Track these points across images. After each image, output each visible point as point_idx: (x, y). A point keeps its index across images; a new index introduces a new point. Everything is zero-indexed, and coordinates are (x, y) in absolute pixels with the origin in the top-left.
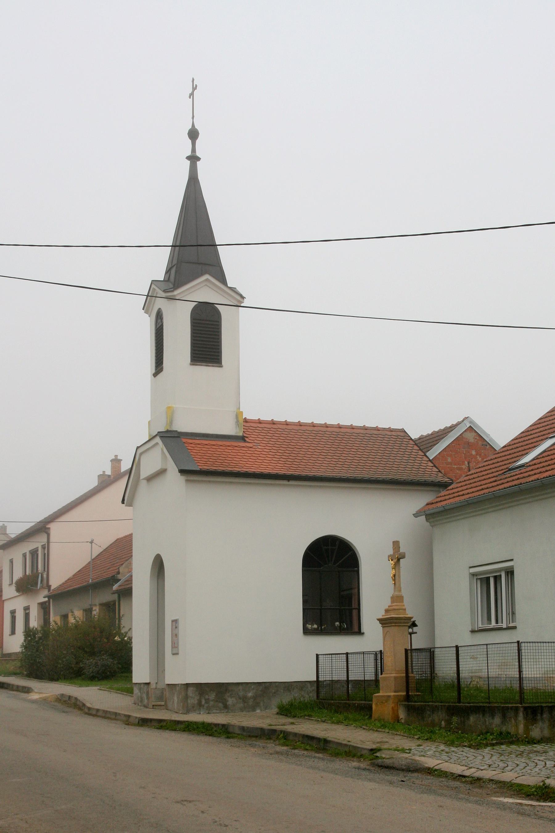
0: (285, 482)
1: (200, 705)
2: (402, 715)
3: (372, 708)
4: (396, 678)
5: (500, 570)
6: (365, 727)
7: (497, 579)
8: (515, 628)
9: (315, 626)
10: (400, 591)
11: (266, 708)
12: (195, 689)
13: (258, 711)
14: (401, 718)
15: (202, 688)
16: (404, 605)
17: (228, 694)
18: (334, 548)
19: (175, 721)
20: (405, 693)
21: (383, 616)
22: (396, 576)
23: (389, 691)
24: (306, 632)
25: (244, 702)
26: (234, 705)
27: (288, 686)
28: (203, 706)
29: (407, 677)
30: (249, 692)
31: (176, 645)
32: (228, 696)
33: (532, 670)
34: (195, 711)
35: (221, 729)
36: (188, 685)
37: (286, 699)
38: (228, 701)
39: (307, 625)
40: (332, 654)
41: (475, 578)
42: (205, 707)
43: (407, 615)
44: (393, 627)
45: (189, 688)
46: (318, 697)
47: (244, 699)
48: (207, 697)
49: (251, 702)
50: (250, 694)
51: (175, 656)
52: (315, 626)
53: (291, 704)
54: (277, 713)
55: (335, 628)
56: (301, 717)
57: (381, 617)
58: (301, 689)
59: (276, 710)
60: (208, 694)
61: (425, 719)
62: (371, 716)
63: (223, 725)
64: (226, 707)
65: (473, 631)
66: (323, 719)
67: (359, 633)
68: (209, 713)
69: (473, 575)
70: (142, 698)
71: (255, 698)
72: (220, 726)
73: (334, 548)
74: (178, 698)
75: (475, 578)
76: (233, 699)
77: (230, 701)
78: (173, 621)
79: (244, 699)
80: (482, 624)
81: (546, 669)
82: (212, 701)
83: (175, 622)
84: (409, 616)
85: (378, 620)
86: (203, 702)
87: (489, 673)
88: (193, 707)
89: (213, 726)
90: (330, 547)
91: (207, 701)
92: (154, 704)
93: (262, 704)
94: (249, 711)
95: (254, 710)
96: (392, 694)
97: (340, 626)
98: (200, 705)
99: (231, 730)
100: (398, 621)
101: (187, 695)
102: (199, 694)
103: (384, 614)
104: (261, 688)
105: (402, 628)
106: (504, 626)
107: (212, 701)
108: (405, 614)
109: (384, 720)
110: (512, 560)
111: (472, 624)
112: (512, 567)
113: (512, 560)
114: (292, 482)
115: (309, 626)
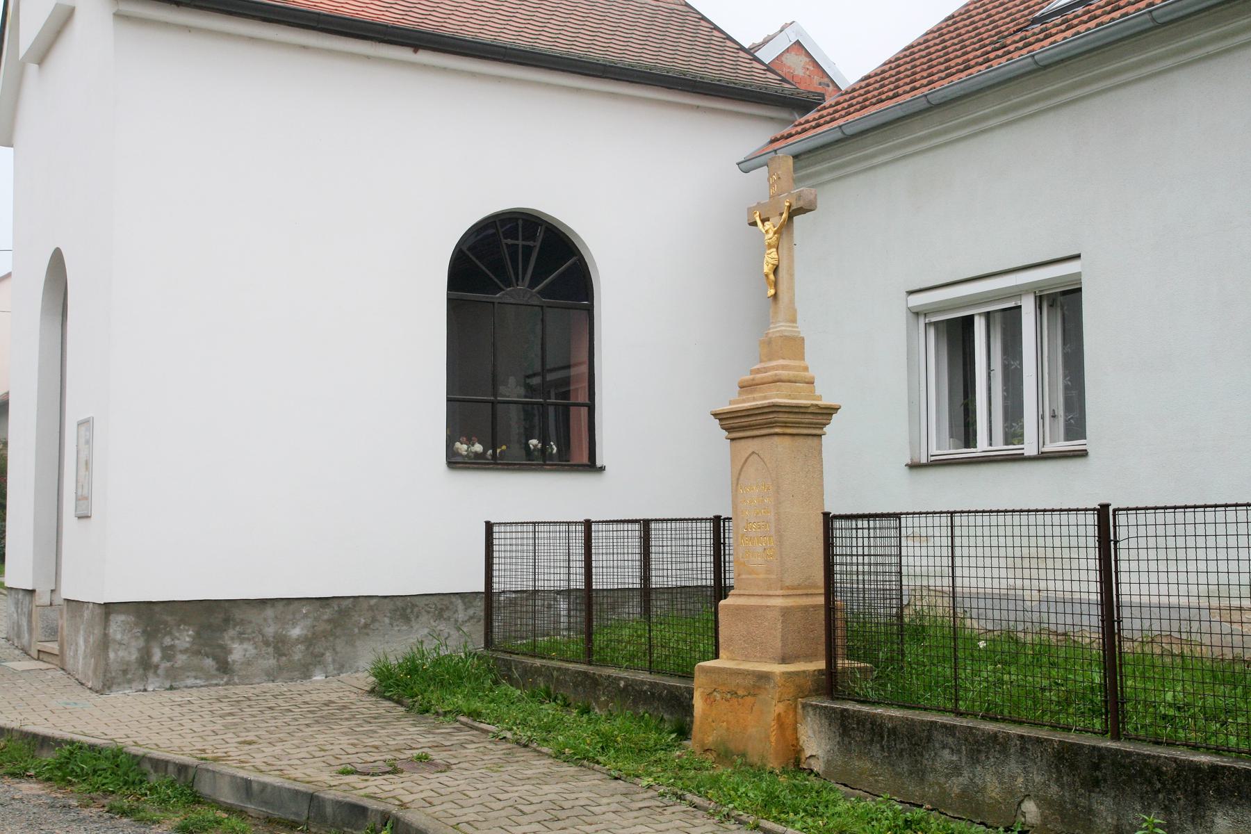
0: (405, 54)
1: (145, 664)
2: (815, 743)
3: (688, 709)
4: (786, 612)
5: (1018, 292)
6: (697, 800)
7: (1008, 322)
8: (1083, 454)
9: (478, 448)
10: (794, 321)
11: (341, 668)
12: (132, 619)
13: (319, 677)
14: (808, 753)
15: (152, 617)
16: (806, 369)
17: (232, 632)
18: (531, 243)
19: (35, 736)
20: (821, 665)
21: (731, 403)
22: (782, 272)
23: (756, 655)
24: (454, 462)
25: (279, 653)
26: (249, 663)
27: (403, 608)
28: (157, 667)
29: (830, 608)
30: (294, 625)
31: (85, 492)
32: (232, 639)
33: (1182, 577)
34: (130, 682)
35: (172, 784)
36: (109, 609)
37: (395, 646)
38: (230, 652)
39: (458, 445)
40: (569, 523)
41: (922, 321)
42: (160, 672)
43: (820, 398)
44: (776, 438)
45: (112, 617)
46: (489, 642)
47: (280, 646)
48: (167, 641)
49: (298, 653)
50: (296, 632)
51: (84, 521)
52: (478, 448)
53: (412, 668)
54: (372, 691)
55: (528, 452)
56: (445, 714)
57: (727, 407)
58: (440, 614)
59: (366, 680)
60: (170, 633)
61: (931, 778)
62: (683, 732)
63: (182, 768)
64: (224, 667)
65: (914, 466)
66: (524, 734)
67: (591, 466)
68: (171, 688)
69: (917, 313)
70: (19, 626)
71: (309, 641)
72: (170, 768)
73: (531, 243)
74: (86, 641)
75: (922, 321)
76: (248, 646)
77: (238, 652)
78: (80, 424)
79: (280, 646)
80: (938, 448)
81: (1213, 578)
82: (185, 651)
83: (85, 423)
84: (825, 402)
85: (715, 415)
86: (157, 656)
87: (958, 582)
88: (125, 672)
89: (147, 767)
90: (520, 242)
91: (169, 652)
92: (40, 646)
93: (329, 657)
94: (292, 680)
95: (306, 674)
96: (778, 669)
97: (543, 451)
98: (145, 664)
99: (205, 788)
100: (792, 418)
101: (106, 635)
102: (144, 632)
103: (735, 396)
104: (328, 614)
105: (800, 441)
106: (1030, 449)
107: (185, 651)
108: (811, 394)
109: (744, 755)
110: (1078, 257)
111: (914, 444)
112: (1077, 277)
113: (1078, 257)
114: (425, 57)
115: (462, 448)
